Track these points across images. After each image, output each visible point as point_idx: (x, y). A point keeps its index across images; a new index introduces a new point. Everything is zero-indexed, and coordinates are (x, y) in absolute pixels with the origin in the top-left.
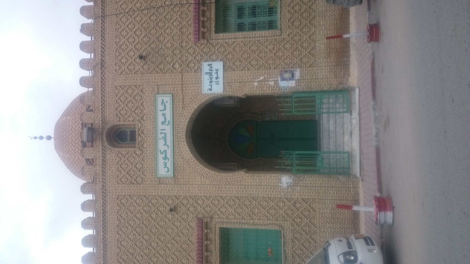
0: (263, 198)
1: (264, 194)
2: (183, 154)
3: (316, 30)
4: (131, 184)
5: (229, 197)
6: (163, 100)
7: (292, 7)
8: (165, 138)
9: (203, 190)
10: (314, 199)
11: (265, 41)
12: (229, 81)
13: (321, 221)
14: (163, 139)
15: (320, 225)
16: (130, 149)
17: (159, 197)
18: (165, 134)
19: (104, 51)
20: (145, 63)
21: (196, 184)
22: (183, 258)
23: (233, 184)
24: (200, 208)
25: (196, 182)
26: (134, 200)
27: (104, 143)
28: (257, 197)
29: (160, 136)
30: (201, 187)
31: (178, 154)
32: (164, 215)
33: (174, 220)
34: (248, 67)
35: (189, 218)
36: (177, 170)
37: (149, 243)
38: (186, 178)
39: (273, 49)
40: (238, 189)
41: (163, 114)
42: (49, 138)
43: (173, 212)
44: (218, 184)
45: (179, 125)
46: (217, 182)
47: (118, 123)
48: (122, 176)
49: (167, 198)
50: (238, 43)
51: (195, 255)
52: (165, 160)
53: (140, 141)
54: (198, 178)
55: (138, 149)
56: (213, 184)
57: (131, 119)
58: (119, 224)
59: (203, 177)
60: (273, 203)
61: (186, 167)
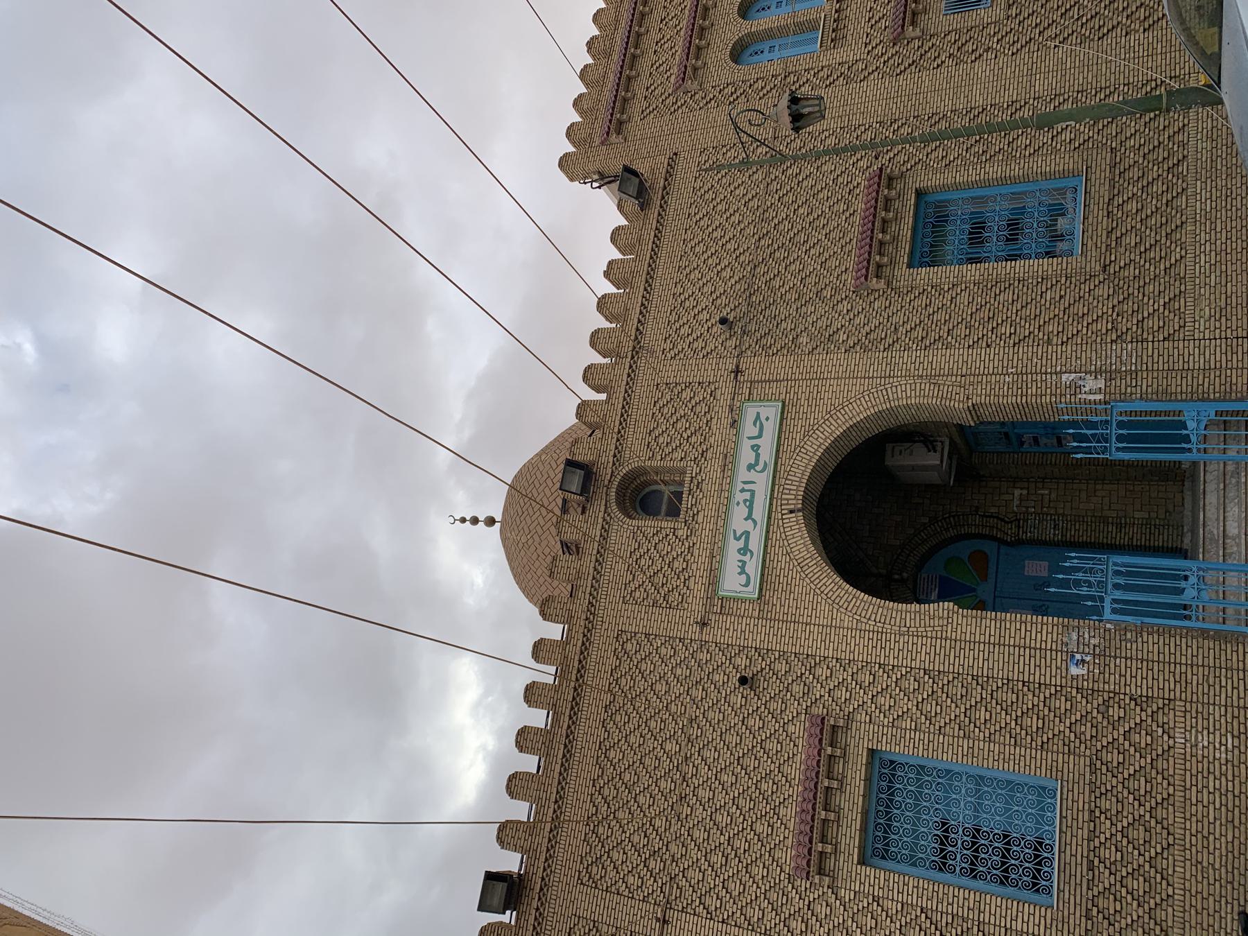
0: (1005, 681)
1: (1011, 669)
2: (789, 544)
3: (1186, 254)
4: (653, 606)
5: (906, 667)
6: (758, 414)
7: (1119, 205)
8: (750, 504)
9: (832, 640)
10: (1169, 700)
11: (1038, 282)
12: (933, 371)
13: (1188, 767)
14: (745, 505)
15: (1185, 781)
16: (664, 524)
17: (716, 646)
18: (753, 492)
19: (647, 312)
20: (730, 336)
21: (817, 623)
22: (759, 820)
23: (920, 634)
24: (819, 689)
25: (817, 619)
26: (655, 647)
27: (610, 507)
28: (988, 677)
29: (740, 497)
30: (828, 632)
31: (778, 542)
32: (724, 695)
33: (746, 711)
34: (989, 340)
35: (787, 713)
36: (769, 583)
37: (676, 765)
38: (791, 605)
39: (1060, 299)
40: (933, 648)
41: (752, 447)
42: (490, 521)
43: (746, 690)
44: (876, 629)
45: (790, 473)
46: (874, 623)
47: (648, 463)
48: (637, 586)
49: (737, 652)
50: (966, 287)
51: (793, 815)
52: (745, 554)
53: (689, 506)
54: (823, 608)
55: (683, 524)
56: (863, 628)
57: (678, 455)
58: (610, 702)
59: (838, 607)
60: (1036, 698)
61: (794, 576)
